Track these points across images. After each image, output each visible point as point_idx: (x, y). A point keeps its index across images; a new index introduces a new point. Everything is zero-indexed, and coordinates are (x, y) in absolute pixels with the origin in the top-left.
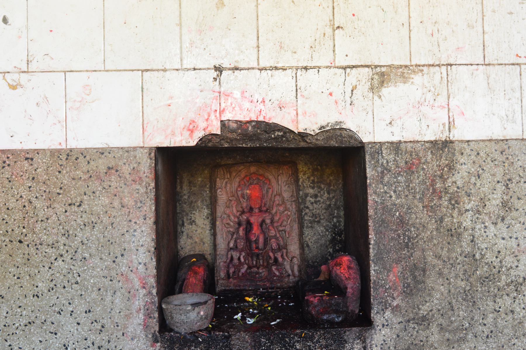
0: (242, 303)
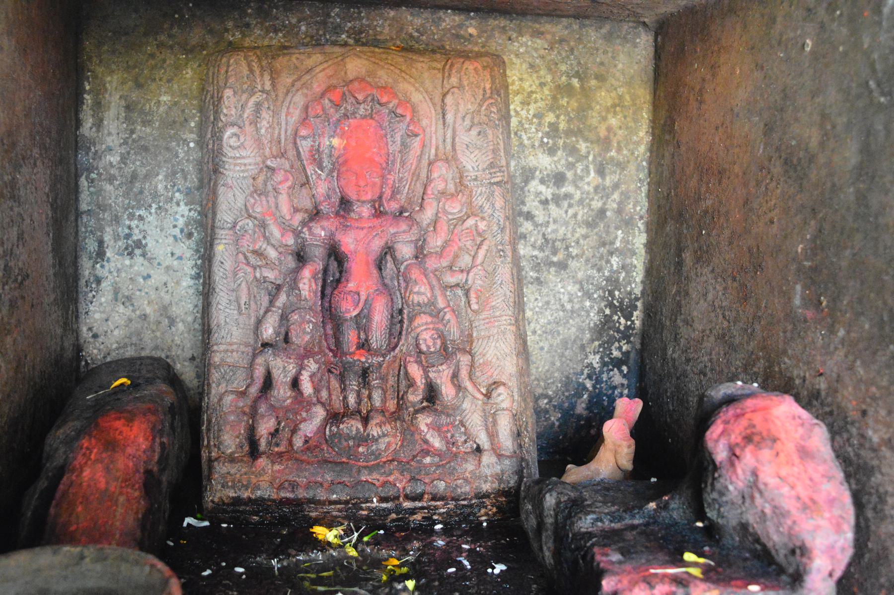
0: (301, 550)
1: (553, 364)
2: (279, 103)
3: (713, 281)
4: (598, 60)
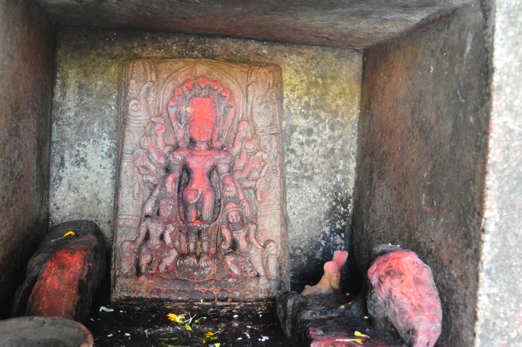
0: (161, 326)
1: (304, 231)
2: (159, 88)
3: (386, 190)
4: (332, 69)
